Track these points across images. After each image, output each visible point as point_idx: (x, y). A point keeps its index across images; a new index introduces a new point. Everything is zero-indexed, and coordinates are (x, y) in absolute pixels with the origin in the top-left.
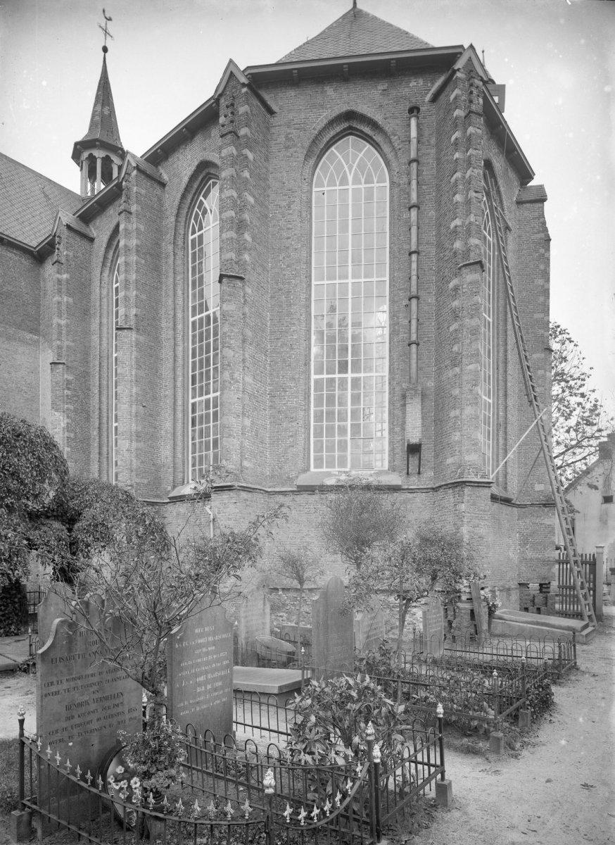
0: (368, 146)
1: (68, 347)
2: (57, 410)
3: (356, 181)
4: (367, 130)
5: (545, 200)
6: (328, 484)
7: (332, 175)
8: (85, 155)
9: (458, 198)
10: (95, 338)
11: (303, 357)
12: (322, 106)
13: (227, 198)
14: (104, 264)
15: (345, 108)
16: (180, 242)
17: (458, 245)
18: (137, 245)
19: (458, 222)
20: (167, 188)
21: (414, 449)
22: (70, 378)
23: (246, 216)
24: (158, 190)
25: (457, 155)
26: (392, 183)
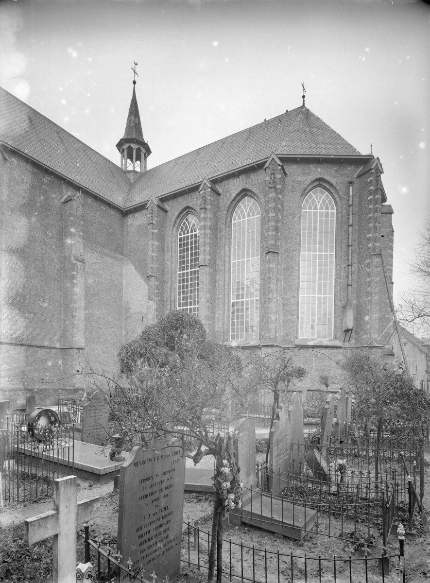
0: (327, 193)
1: (157, 268)
2: (151, 300)
3: (321, 208)
4: (327, 186)
5: (393, 213)
6: (310, 344)
7: (310, 204)
8: (127, 146)
9: (371, 225)
10: (168, 263)
11: (297, 287)
12: (309, 174)
13: (272, 216)
14: (174, 226)
15: (319, 176)
16: (228, 224)
17: (370, 245)
18: (210, 226)
19: (371, 235)
20: (221, 197)
21: (347, 331)
22: (157, 283)
23: (279, 225)
24: (217, 197)
25: (371, 206)
26: (337, 212)
